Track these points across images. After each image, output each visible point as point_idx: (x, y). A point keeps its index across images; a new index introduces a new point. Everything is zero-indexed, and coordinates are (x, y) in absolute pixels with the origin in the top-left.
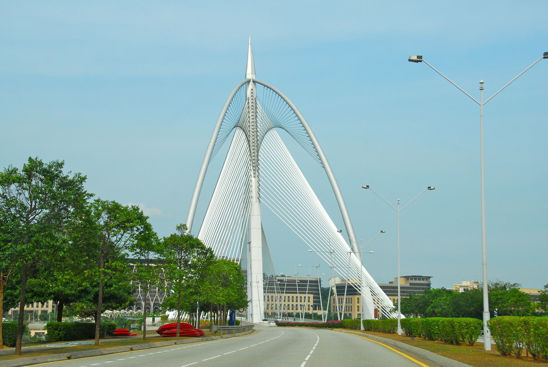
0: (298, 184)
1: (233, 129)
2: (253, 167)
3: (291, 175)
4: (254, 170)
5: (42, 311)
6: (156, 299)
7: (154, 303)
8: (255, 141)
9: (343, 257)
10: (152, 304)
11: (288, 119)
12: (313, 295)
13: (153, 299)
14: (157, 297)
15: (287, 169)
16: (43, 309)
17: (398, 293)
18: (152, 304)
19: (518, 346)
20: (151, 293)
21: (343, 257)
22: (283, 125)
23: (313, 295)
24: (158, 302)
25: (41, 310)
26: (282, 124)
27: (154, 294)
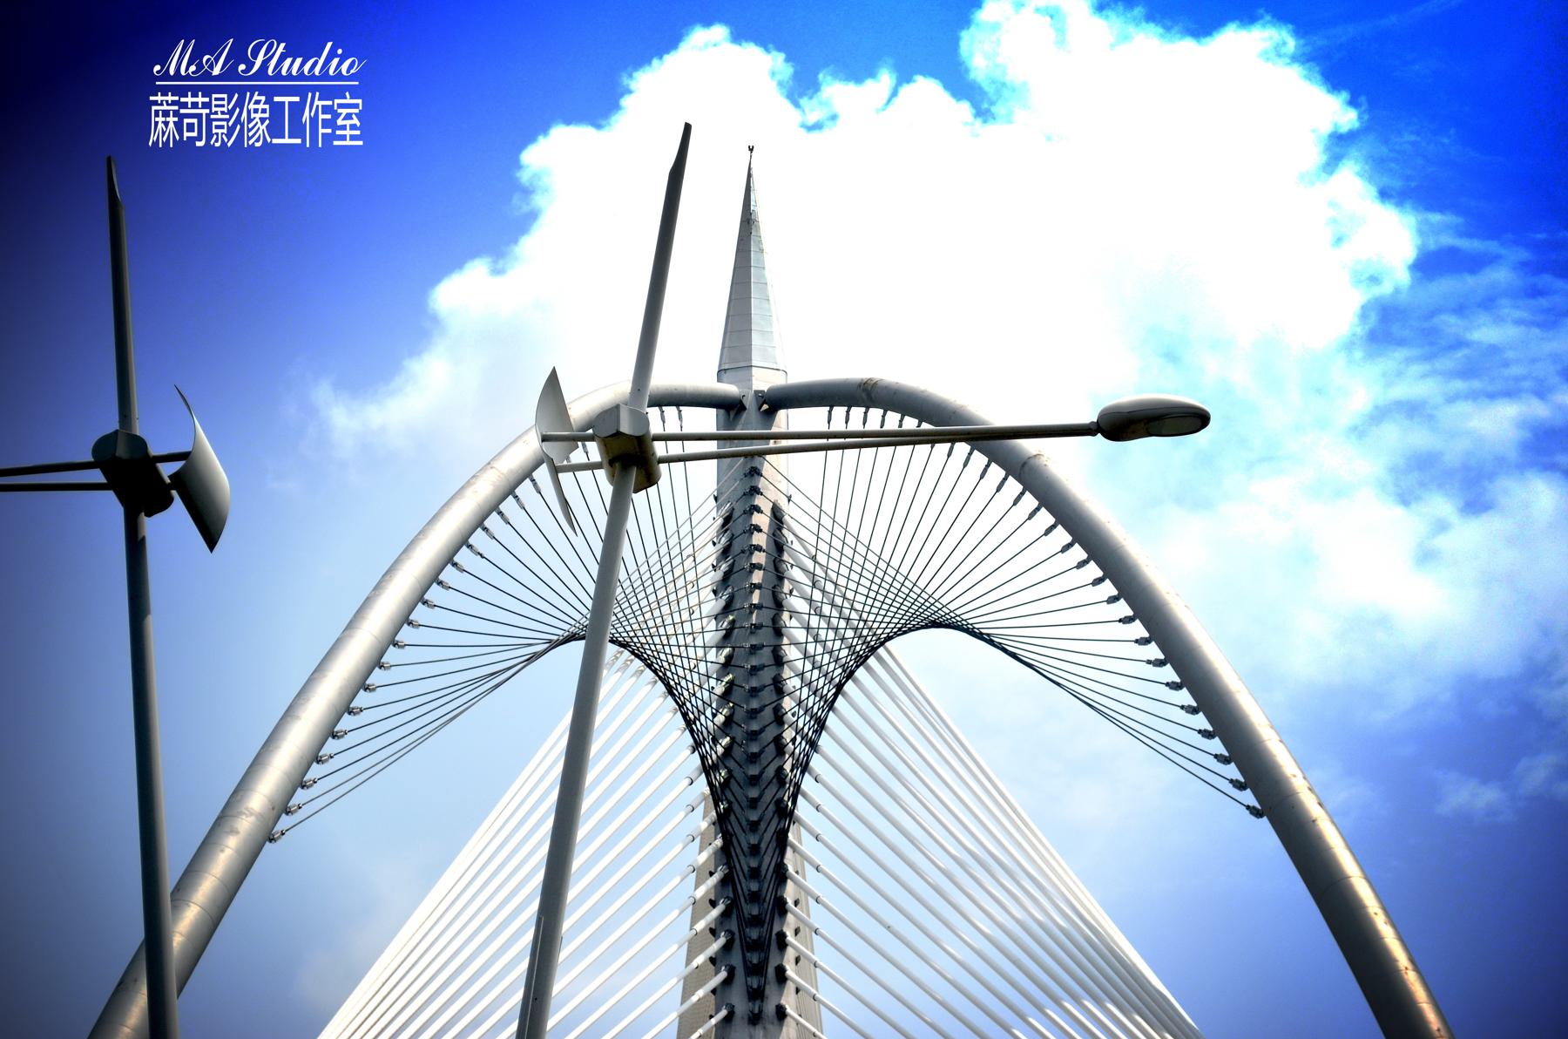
8: (762, 752)
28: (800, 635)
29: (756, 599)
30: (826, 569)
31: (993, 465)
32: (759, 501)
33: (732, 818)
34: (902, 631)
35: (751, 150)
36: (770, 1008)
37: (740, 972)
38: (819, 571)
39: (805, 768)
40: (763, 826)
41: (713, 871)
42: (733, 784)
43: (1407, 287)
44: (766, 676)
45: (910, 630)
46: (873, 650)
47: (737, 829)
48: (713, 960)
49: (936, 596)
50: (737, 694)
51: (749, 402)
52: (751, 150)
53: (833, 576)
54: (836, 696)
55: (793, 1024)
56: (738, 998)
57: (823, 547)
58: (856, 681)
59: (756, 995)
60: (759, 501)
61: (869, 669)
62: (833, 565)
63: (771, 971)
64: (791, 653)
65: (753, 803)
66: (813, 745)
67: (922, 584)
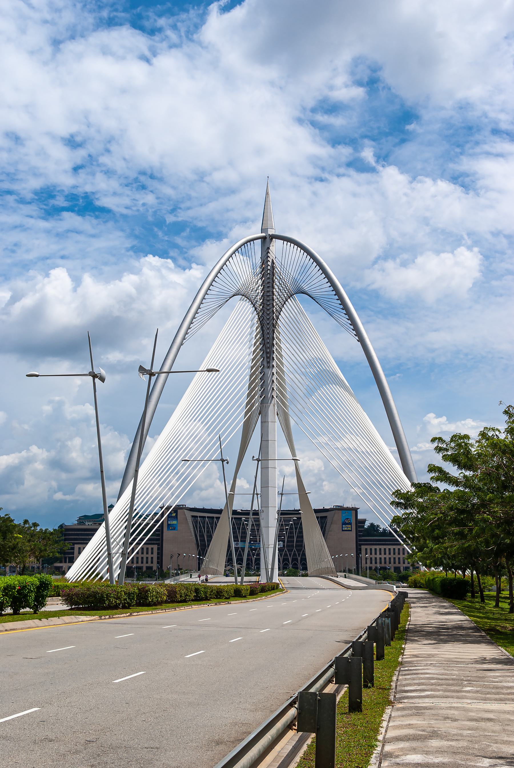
0: (357, 414)
1: (230, 298)
2: (267, 353)
3: (349, 403)
4: (268, 358)
5: (148, 568)
6: (285, 554)
7: (283, 559)
8: (270, 313)
9: (356, 420)
10: (299, 559)
11: (309, 278)
12: (157, 545)
13: (282, 554)
14: (286, 551)
15: (349, 403)
16: (148, 565)
17: (69, 563)
18: (299, 559)
19: (475, 572)
20: (288, 547)
21: (342, 392)
22: (306, 288)
23: (157, 545)
24: (296, 557)
25: (146, 566)
26: (305, 288)
27: (301, 548)
28: (278, 284)
29: (269, 272)
30: (286, 282)
31: (295, 246)
32: (269, 259)
33: (264, 327)
34: (296, 293)
35: (268, 177)
36: (271, 365)
37: (265, 358)
38: (285, 282)
39: (278, 318)
40: (270, 328)
41: (243, 593)
42: (264, 320)
43: (468, 284)
44: (271, 297)
45: (298, 293)
46: (291, 296)
47: (265, 330)
48: (260, 350)
49: (303, 287)
50: (266, 288)
51: (268, 237)
52: (268, 177)
53: (287, 283)
54: (284, 304)
55: (275, 369)
56: (265, 363)
57: (286, 278)
58: (286, 304)
59: (268, 362)
60: (269, 259)
61: (290, 299)
62: (287, 281)
63: (271, 358)
64: (276, 287)
65: (268, 324)
66: (280, 314)
67: (302, 286)
